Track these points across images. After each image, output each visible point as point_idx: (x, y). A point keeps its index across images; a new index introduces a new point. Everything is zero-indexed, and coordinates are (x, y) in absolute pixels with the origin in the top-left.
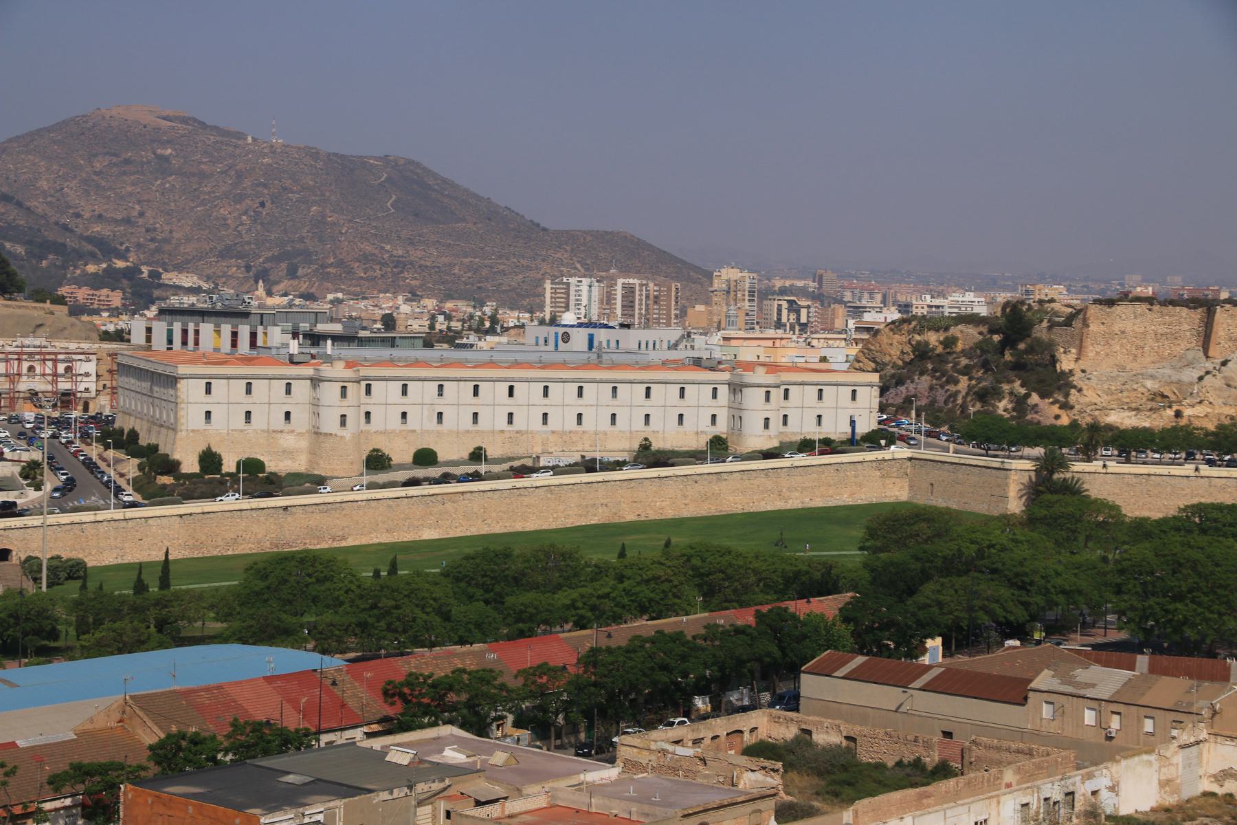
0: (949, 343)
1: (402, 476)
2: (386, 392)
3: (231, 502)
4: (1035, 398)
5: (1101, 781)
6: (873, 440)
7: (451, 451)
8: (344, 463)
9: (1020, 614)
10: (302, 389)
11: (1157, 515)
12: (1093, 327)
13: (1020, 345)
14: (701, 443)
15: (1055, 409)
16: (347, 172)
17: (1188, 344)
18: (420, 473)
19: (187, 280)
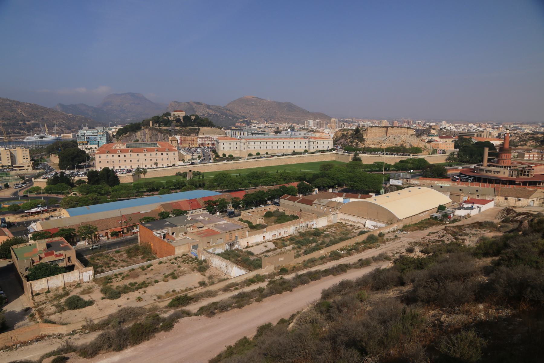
0: (347, 133)
1: (253, 157)
3: (225, 162)
5: (314, 222)
6: (331, 150)
7: (262, 153)
8: (245, 155)
9: (332, 184)
11: (372, 163)
13: (358, 134)
14: (303, 151)
16: (279, 104)
17: (384, 133)
18: (249, 158)
19: (255, 122)
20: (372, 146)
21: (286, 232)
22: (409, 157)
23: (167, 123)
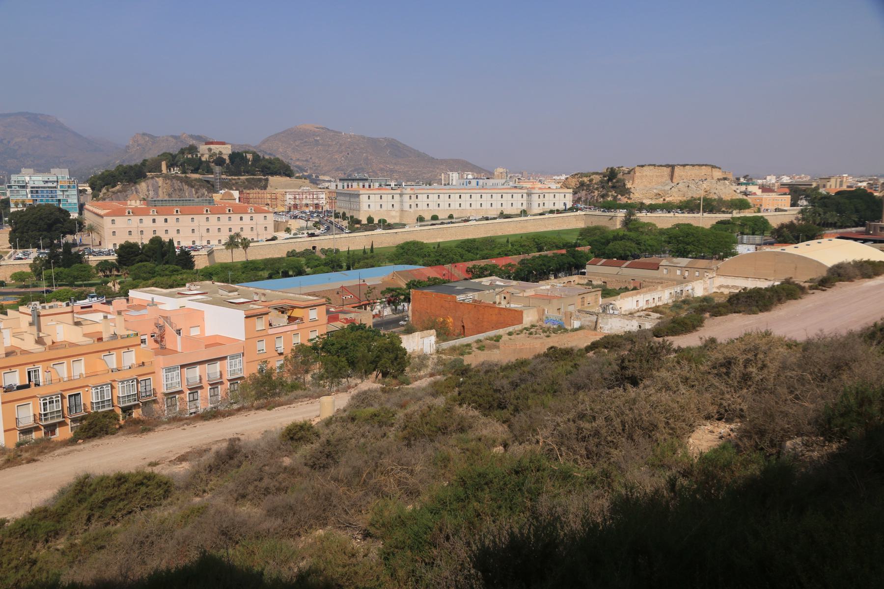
0: (591, 181)
2: (422, 198)
3: (379, 231)
4: (619, 196)
5: (689, 287)
8: (410, 219)
10: (397, 197)
11: (670, 226)
12: (637, 174)
13: (613, 180)
14: (519, 212)
15: (626, 200)
16: (374, 144)
17: (667, 178)
18: (434, 222)
19: (327, 178)
20: (647, 202)
21: (660, 298)
22: (730, 216)
23: (198, 166)
